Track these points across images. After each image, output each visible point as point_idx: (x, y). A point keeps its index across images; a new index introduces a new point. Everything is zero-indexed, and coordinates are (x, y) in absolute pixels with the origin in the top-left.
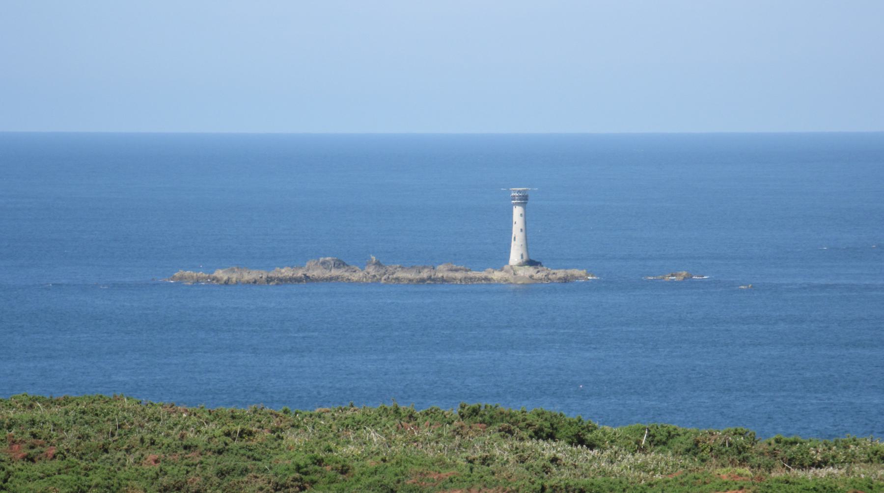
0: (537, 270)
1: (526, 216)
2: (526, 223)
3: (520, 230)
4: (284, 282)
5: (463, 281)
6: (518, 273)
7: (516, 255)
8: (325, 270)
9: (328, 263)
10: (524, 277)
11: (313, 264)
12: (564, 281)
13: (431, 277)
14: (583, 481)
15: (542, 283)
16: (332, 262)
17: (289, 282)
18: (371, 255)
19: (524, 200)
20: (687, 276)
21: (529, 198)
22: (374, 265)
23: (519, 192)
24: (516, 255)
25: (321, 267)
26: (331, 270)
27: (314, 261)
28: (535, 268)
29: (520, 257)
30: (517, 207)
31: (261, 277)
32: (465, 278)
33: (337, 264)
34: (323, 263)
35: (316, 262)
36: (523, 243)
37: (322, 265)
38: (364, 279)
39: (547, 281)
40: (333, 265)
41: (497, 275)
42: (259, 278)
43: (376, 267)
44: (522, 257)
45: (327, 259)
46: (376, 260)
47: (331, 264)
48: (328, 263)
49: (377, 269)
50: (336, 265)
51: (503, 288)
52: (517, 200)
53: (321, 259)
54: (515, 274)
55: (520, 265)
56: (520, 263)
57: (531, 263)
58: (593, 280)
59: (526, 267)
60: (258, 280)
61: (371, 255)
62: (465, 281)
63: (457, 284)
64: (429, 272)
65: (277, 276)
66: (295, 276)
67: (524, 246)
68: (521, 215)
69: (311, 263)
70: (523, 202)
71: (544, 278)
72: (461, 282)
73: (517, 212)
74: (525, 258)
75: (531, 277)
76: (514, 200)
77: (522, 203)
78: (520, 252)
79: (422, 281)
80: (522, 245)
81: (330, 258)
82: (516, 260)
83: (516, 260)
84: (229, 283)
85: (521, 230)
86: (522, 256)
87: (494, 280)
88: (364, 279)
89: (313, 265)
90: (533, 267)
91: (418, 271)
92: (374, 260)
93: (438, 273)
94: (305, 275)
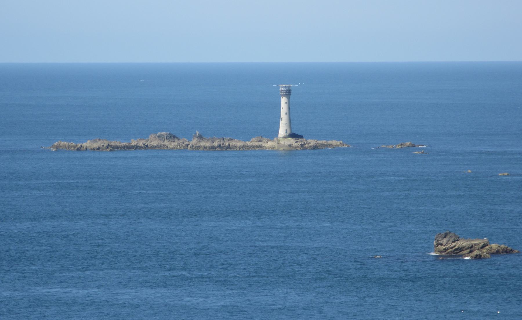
0: (296, 141)
1: (289, 104)
2: (289, 109)
3: (285, 114)
4: (120, 149)
5: (241, 148)
6: (280, 142)
7: (282, 131)
8: (161, 141)
9: (163, 136)
10: (284, 145)
11: (153, 137)
12: (313, 148)
13: (220, 145)
14: (442, 255)
15: (297, 150)
16: (165, 136)
17: (123, 149)
18: (197, 131)
19: (288, 93)
20: (410, 146)
21: (292, 91)
22: (197, 137)
23: (285, 87)
24: (282, 131)
25: (158, 139)
26: (164, 141)
27: (154, 135)
28: (295, 139)
29: (285, 132)
30: (283, 97)
31: (103, 146)
32: (243, 146)
33: (168, 137)
34: (159, 136)
35: (155, 135)
36: (288, 122)
37: (158, 138)
38: (178, 147)
39: (300, 148)
40: (166, 138)
41: (270, 144)
42: (102, 146)
43: (198, 139)
44: (286, 132)
45: (163, 133)
46: (199, 134)
47: (165, 137)
48: (163, 136)
49: (199, 140)
50: (168, 138)
51: (273, 153)
52: (283, 93)
53: (159, 134)
54: (278, 143)
55: (285, 137)
56: (285, 136)
57: (293, 135)
58: (416, 152)
59: (289, 139)
60: (101, 147)
61: (197, 131)
62: (243, 148)
63: (237, 150)
64: (219, 142)
65: (116, 145)
66: (138, 145)
67: (288, 124)
68: (286, 103)
69: (152, 136)
70: (287, 94)
71: (299, 146)
72: (240, 148)
73: (284, 100)
74: (289, 132)
75: (290, 145)
76: (281, 93)
77: (286, 95)
78: (285, 129)
79: (213, 148)
80: (286, 124)
81: (164, 133)
82: (282, 134)
83: (282, 134)
84: (81, 150)
85: (286, 113)
86: (286, 131)
87: (266, 148)
88: (178, 147)
89: (153, 138)
90: (294, 139)
91: (212, 141)
92: (198, 134)
93: (226, 143)
94: (144, 144)
